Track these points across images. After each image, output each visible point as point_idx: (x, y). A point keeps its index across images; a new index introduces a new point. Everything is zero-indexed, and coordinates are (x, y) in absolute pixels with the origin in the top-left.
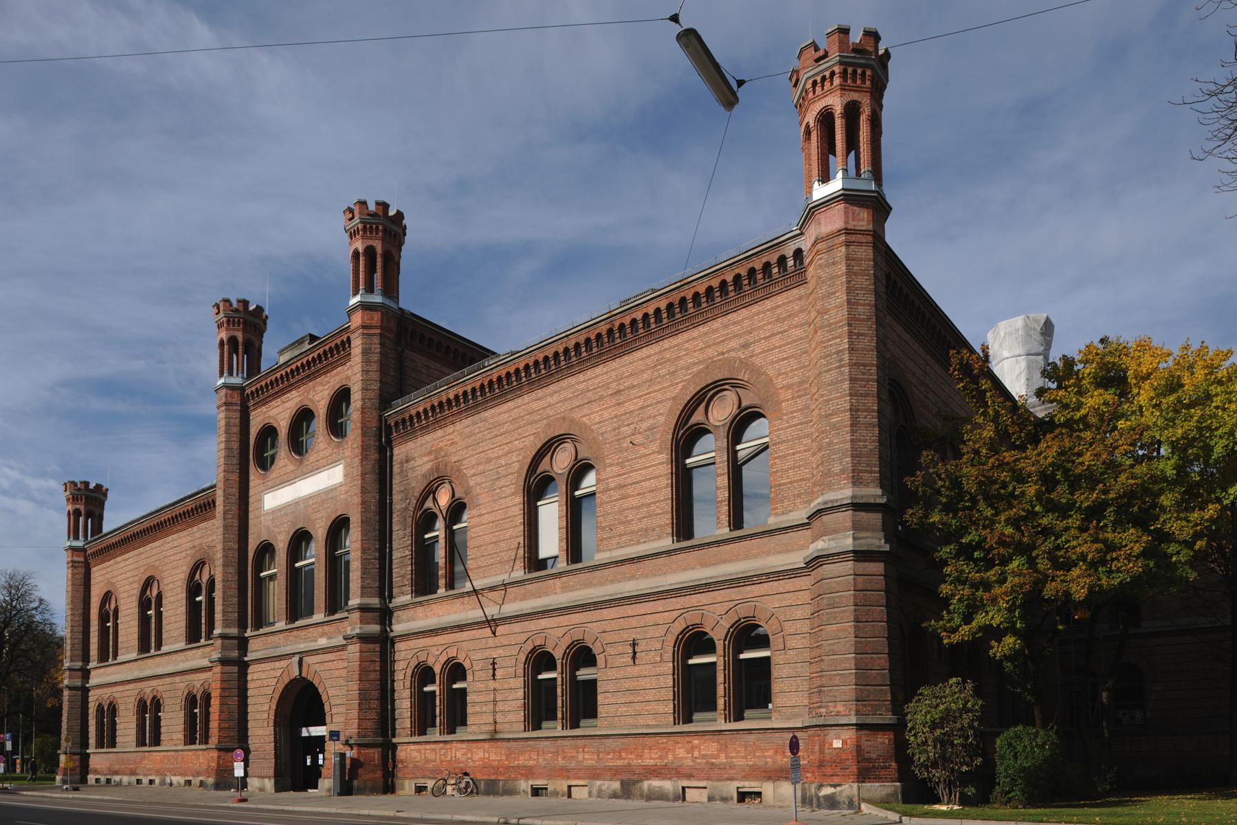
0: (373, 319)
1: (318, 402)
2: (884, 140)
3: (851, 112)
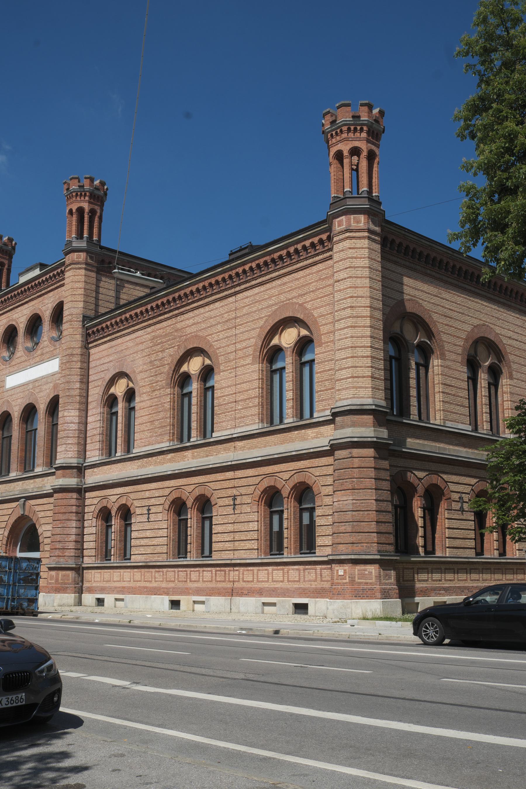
0: (80, 258)
1: (45, 311)
2: (102, 224)
3: (92, 212)
